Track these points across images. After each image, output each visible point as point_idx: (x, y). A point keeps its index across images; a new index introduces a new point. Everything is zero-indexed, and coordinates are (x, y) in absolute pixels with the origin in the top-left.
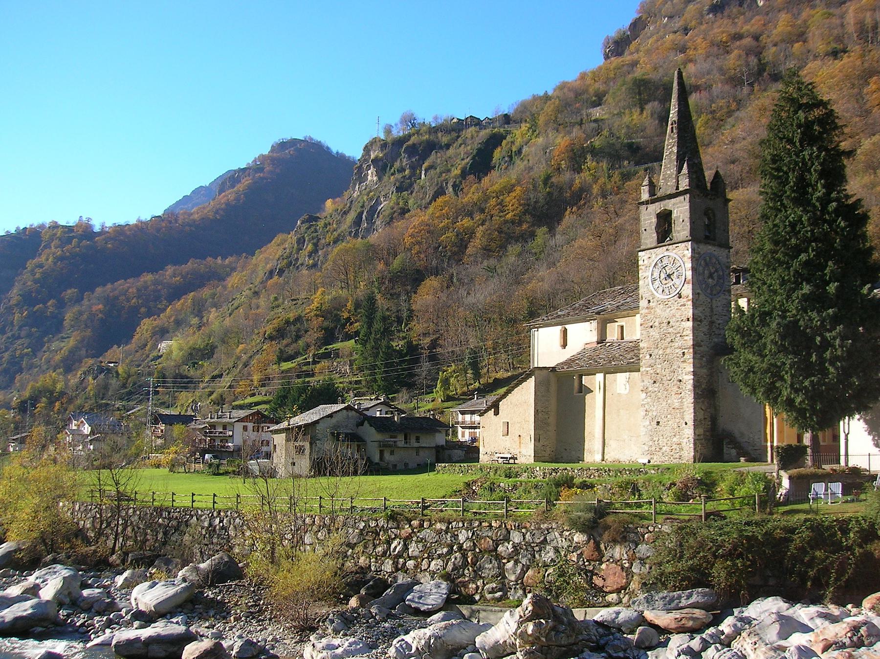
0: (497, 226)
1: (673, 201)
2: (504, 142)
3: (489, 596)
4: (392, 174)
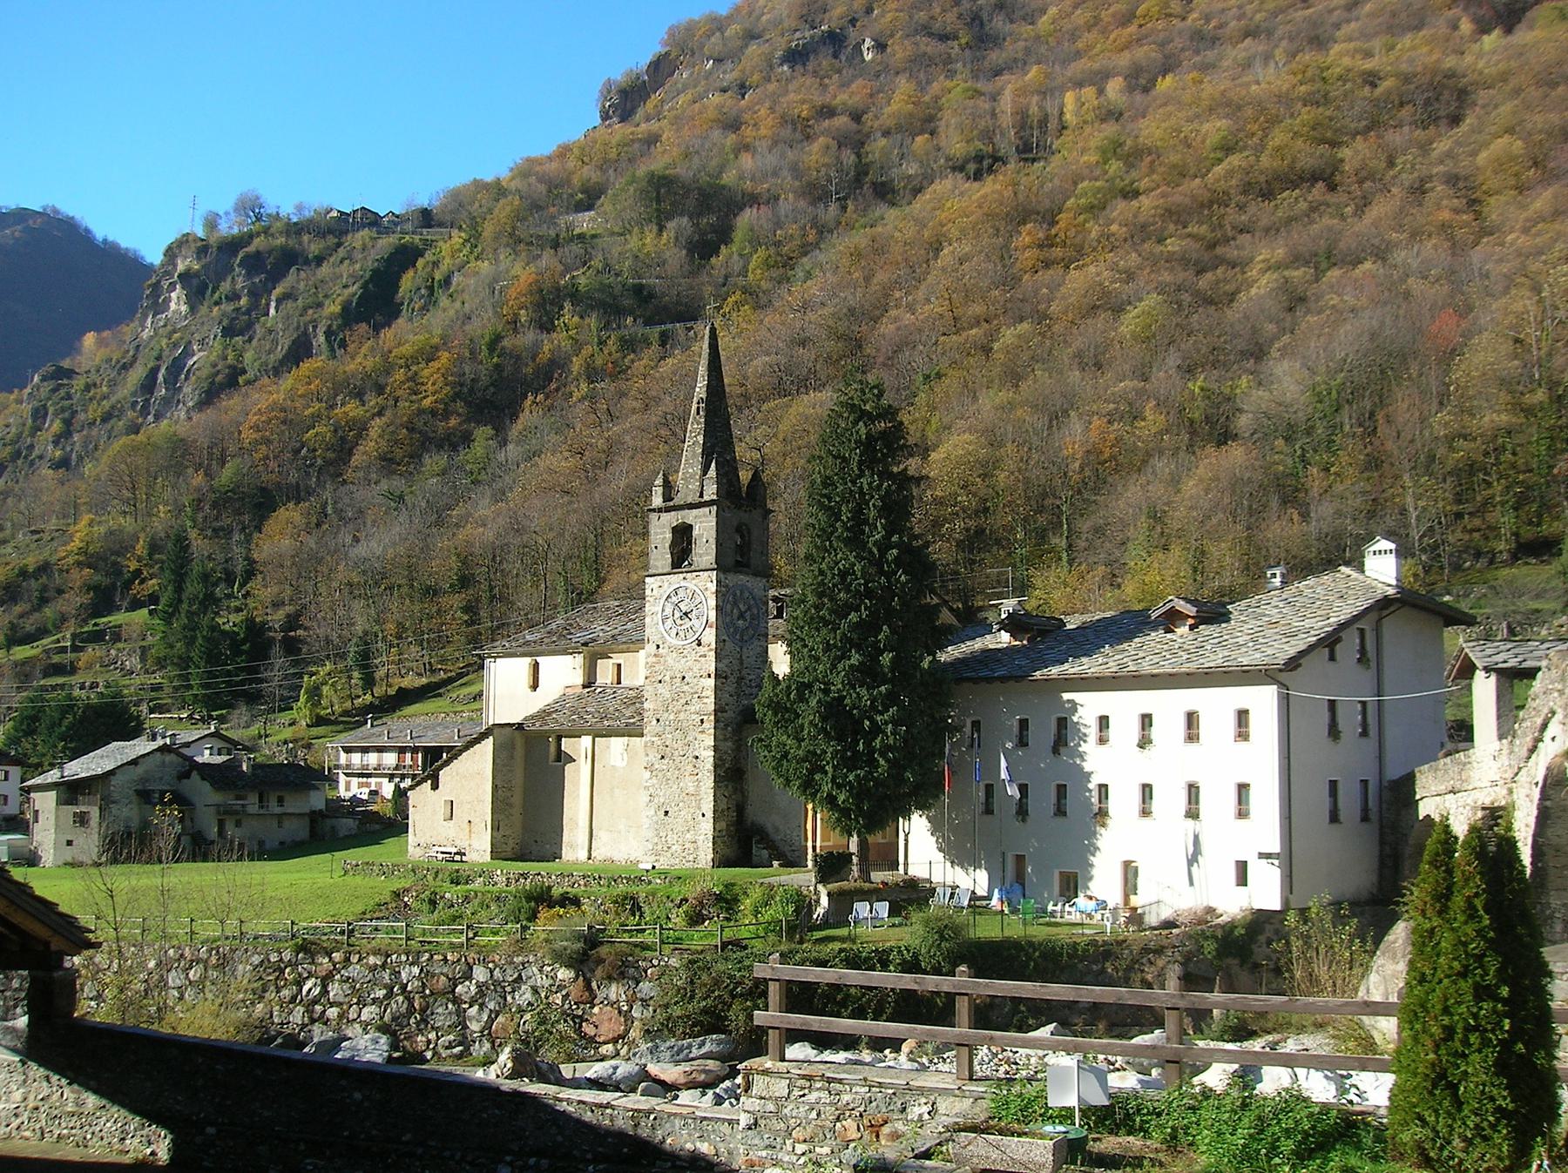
0: (405, 419)
1: (695, 512)
2: (420, 263)
3: (444, 1053)
4: (217, 303)
